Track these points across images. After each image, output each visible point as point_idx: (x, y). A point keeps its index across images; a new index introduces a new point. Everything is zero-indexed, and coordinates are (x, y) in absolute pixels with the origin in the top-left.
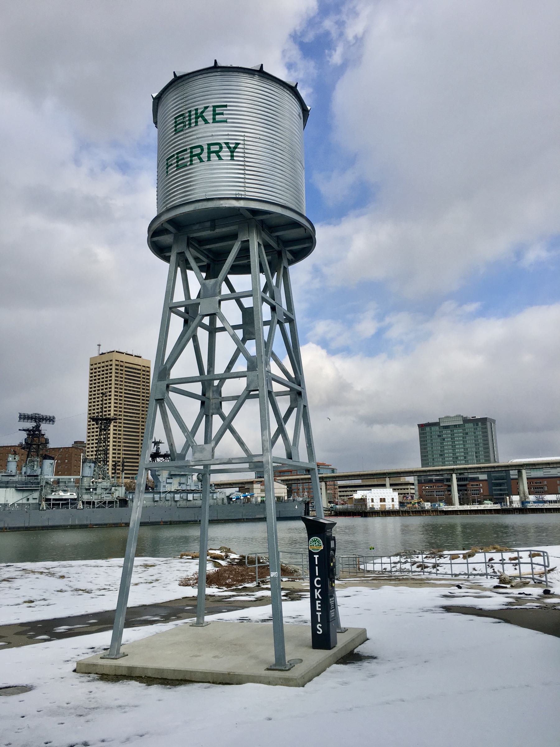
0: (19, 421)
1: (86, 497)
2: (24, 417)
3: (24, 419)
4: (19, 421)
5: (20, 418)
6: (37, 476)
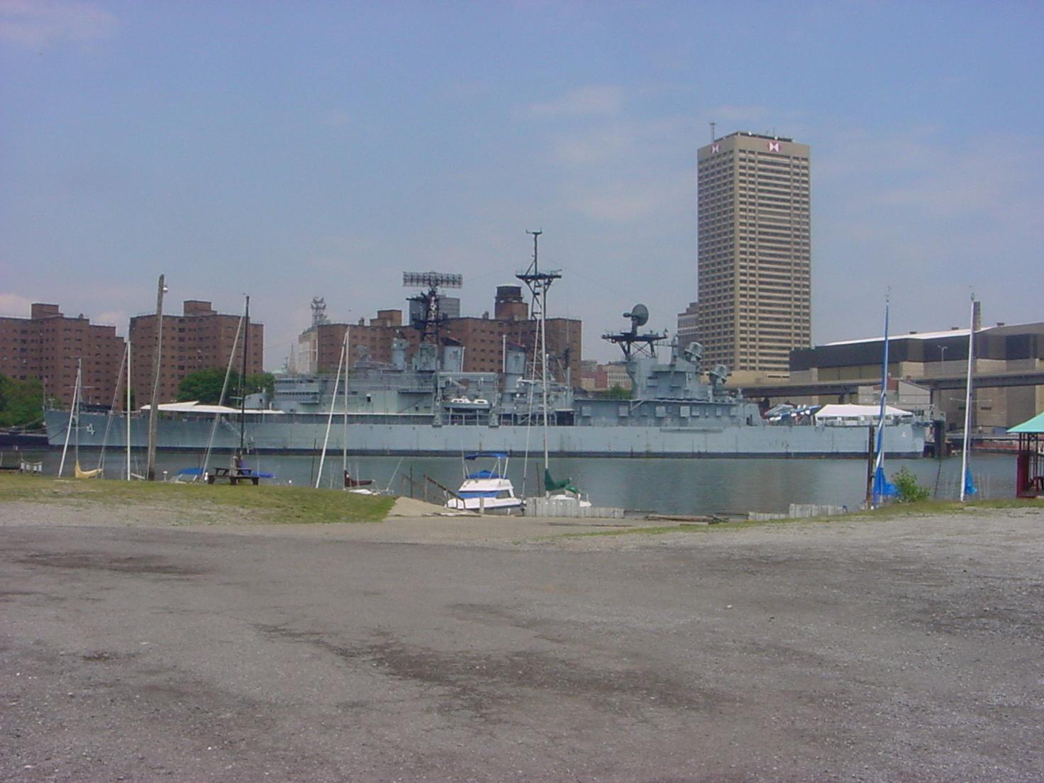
0: (405, 285)
1: (508, 408)
2: (411, 279)
3: (412, 280)
4: (405, 285)
5: (405, 281)
6: (433, 372)
